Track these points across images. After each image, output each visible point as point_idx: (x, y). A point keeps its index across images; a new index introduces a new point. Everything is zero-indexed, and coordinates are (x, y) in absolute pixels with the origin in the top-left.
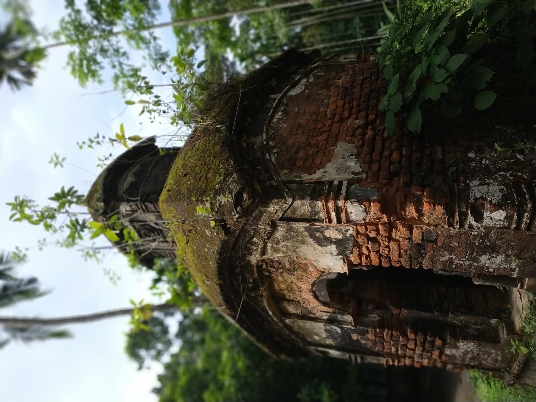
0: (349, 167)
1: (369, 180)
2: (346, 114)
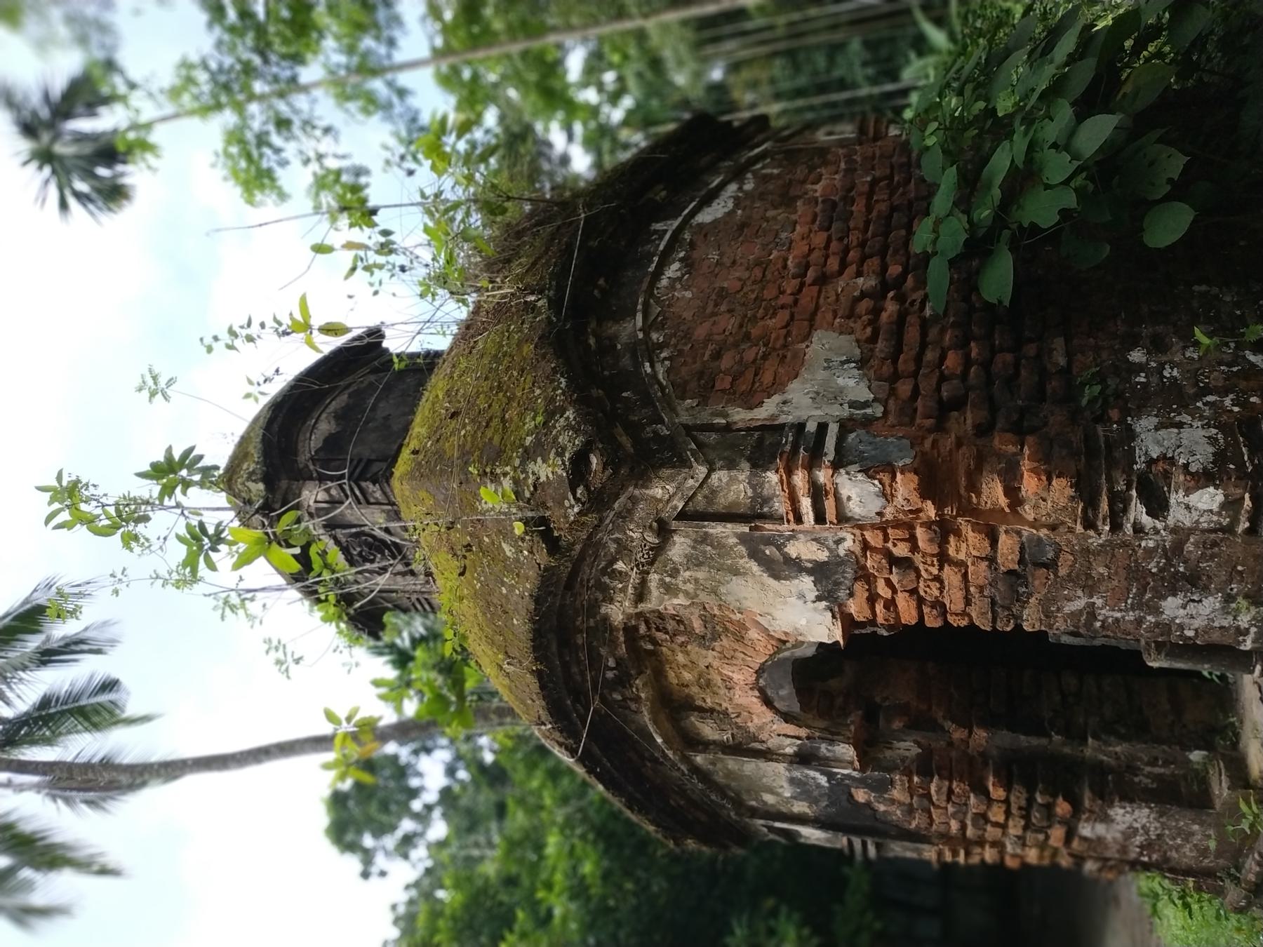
1: (891, 419)
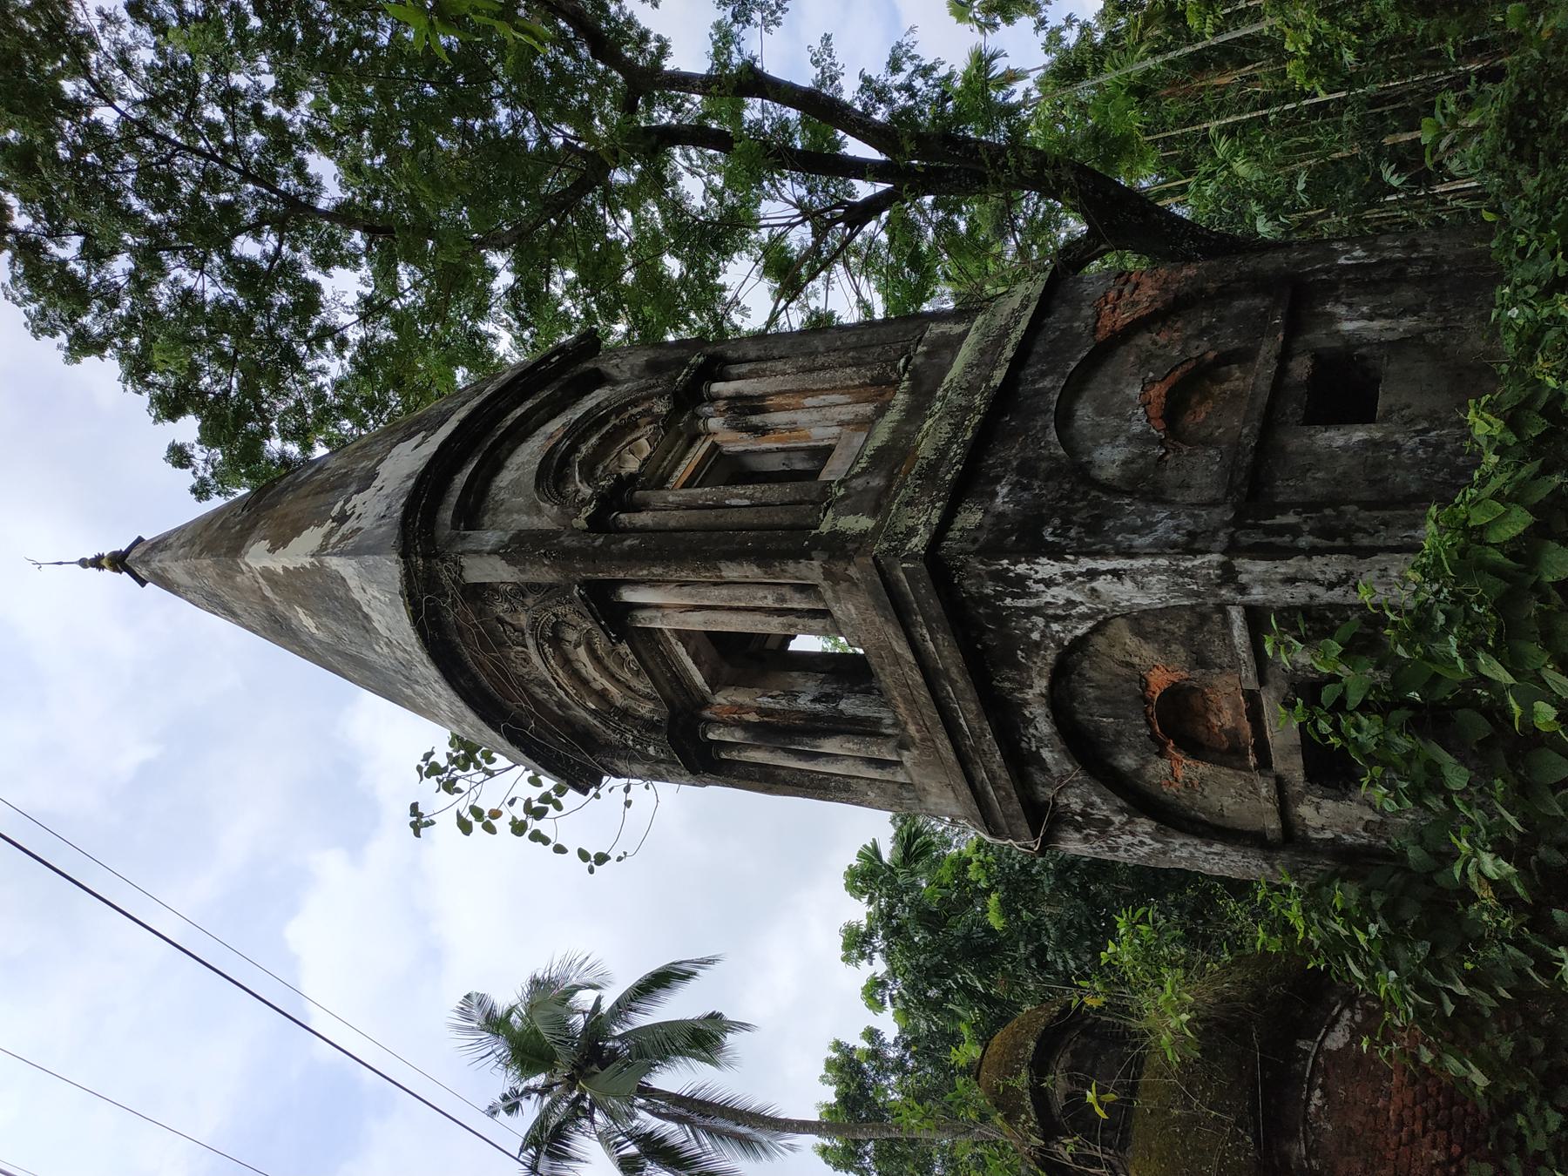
2: (1418, 1128)
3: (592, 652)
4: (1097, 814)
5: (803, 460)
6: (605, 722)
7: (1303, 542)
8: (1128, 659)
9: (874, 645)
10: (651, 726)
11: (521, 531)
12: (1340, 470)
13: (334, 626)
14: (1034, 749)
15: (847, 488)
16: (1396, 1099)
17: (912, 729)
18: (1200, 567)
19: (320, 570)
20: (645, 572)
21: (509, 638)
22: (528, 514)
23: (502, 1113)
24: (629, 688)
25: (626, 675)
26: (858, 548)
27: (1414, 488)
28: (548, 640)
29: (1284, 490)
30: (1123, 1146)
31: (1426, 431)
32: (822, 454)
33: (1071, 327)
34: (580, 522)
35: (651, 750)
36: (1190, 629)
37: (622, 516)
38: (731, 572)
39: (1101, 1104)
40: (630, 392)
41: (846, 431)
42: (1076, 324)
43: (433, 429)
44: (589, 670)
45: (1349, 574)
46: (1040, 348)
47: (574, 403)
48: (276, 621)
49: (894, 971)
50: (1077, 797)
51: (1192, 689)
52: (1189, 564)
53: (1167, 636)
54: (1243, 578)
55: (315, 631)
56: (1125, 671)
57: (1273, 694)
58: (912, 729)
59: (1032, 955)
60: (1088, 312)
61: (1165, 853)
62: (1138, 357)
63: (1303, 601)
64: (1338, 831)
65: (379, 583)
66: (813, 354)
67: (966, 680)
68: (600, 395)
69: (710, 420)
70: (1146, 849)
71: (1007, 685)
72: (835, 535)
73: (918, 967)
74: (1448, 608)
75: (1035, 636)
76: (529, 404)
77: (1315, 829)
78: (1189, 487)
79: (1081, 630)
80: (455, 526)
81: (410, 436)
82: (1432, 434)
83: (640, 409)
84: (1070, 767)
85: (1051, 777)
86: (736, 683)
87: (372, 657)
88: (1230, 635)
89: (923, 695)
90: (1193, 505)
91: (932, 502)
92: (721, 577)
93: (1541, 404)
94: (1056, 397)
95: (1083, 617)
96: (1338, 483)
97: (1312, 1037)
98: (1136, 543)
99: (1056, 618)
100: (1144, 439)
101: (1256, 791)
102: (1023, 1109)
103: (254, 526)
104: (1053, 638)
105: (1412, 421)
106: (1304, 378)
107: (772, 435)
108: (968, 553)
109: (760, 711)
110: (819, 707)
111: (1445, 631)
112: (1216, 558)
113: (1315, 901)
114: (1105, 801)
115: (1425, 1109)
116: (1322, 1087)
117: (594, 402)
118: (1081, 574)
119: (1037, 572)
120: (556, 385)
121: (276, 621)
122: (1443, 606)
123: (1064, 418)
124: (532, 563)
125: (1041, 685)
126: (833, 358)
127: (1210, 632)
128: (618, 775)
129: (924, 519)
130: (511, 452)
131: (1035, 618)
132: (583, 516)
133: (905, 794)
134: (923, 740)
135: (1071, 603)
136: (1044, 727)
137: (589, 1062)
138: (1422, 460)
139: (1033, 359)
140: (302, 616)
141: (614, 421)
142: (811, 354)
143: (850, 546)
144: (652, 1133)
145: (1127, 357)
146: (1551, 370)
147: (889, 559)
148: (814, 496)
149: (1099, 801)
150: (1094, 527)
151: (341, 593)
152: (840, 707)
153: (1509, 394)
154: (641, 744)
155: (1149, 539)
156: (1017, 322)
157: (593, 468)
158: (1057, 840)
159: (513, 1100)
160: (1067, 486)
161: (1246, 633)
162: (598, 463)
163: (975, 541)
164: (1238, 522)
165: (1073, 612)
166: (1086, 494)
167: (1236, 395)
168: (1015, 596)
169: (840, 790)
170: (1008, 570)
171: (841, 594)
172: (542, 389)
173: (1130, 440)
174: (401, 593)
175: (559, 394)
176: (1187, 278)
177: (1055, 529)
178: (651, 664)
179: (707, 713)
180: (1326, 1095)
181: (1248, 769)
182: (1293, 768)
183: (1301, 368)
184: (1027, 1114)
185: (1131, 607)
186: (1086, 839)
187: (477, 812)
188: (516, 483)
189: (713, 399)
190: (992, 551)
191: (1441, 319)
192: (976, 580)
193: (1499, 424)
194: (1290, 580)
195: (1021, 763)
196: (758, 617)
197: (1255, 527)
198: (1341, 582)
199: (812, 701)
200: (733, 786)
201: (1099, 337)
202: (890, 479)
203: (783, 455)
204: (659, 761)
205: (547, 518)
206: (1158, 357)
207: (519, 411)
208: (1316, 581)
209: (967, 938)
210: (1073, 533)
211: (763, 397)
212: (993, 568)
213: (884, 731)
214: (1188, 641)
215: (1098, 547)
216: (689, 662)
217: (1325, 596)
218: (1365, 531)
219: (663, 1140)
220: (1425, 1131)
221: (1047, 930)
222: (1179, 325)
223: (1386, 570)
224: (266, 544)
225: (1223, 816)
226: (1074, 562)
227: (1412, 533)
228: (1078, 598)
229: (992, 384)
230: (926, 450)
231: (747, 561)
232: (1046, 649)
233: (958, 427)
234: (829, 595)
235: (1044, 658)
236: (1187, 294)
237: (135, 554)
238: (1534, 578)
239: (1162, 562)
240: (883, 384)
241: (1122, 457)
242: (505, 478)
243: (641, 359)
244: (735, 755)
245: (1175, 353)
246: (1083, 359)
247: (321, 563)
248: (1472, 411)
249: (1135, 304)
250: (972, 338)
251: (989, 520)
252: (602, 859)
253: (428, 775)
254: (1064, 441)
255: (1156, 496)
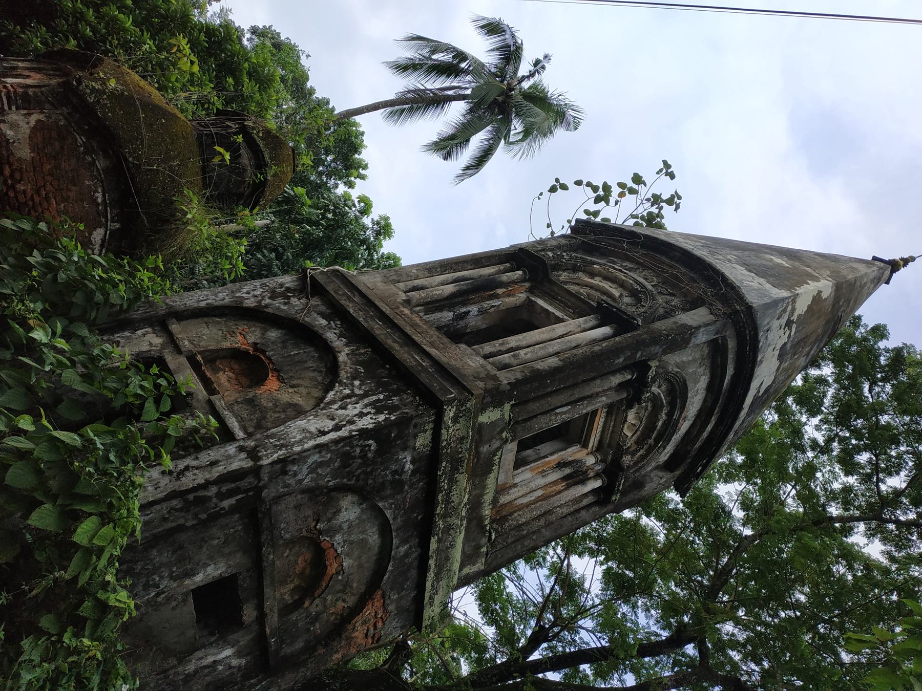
0: (10, 129)
2: (37, 199)
3: (610, 296)
4: (280, 300)
5: (528, 456)
6: (584, 260)
7: (214, 490)
8: (296, 389)
9: (449, 348)
10: (557, 267)
11: (686, 347)
12: (205, 549)
13: (764, 262)
14: (332, 322)
15: (502, 439)
16: (54, 213)
17: (407, 311)
18: (273, 454)
19: (789, 288)
20: (604, 345)
21: (662, 287)
22: (683, 362)
23: (542, 58)
24: (578, 284)
25: (583, 291)
26: (483, 399)
27: (155, 552)
28: (640, 292)
29: (236, 524)
30: (200, 137)
31: (157, 595)
32: (519, 463)
33: (398, 594)
34: (653, 364)
35: (551, 254)
36: (265, 418)
37: (629, 377)
38: (554, 362)
39: (220, 153)
40: (648, 463)
41: (511, 482)
42: (396, 596)
43: (756, 398)
44: (606, 285)
45: (178, 478)
46: (414, 573)
47: (677, 446)
48: (795, 257)
49: (357, 219)
50: (296, 305)
51: (250, 387)
52: (280, 453)
53: (277, 409)
54: (243, 455)
55: (772, 257)
56: (295, 382)
57: (200, 397)
58: (407, 311)
59: (283, 254)
60: (391, 608)
61: (233, 292)
62: (351, 587)
63: (201, 454)
64: (134, 336)
65: (754, 289)
66: (548, 525)
67: (388, 345)
68: (664, 457)
69: (594, 461)
70: (244, 291)
71: (362, 351)
72: (499, 404)
73: (344, 227)
74: (110, 466)
75: (357, 383)
76: (705, 434)
77: (148, 333)
78: (295, 507)
79: (331, 395)
80: (724, 338)
81: (767, 390)
82: (153, 594)
83: (639, 454)
84: (307, 319)
85: (315, 311)
86: (517, 308)
87: (734, 252)
88: (239, 422)
89: (409, 330)
90: (290, 494)
91: (449, 444)
92: (558, 357)
93: (89, 625)
94: (394, 542)
95: (333, 402)
96: (203, 540)
97: (112, 232)
98: (318, 456)
99: (348, 396)
100: (332, 531)
101: (191, 342)
102: (262, 139)
103: (834, 305)
104: (346, 385)
105: (169, 599)
106: (245, 607)
107: (554, 464)
108: (417, 416)
109: (497, 296)
110: (464, 310)
111: (107, 451)
112: (265, 462)
113: (137, 294)
114: (279, 308)
115: (36, 211)
116: (98, 204)
117: (666, 451)
118: (344, 426)
119: (371, 418)
120: (693, 453)
121: (795, 257)
122: (113, 466)
123: (385, 530)
124: (672, 329)
125: (342, 357)
126: (535, 526)
127: (251, 420)
128: (563, 236)
129: (451, 431)
130: (705, 401)
131: (361, 392)
132: (654, 368)
133: (395, 278)
134: (398, 308)
135: (343, 407)
136: (330, 336)
137: (504, 102)
138: (154, 574)
139: (416, 563)
140: (784, 263)
141: (651, 441)
142: (548, 525)
143: (488, 399)
144: (455, 77)
145: (358, 585)
146: (89, 650)
147: (463, 397)
148: (519, 428)
149: (282, 307)
150: (346, 458)
151: (771, 279)
152: (452, 313)
153: (111, 628)
154: (558, 255)
155: (310, 461)
156: (432, 585)
157: (654, 406)
158: (299, 279)
159: (538, 67)
160: (370, 482)
161: (230, 425)
162: (652, 411)
163: (415, 426)
164: (258, 490)
165: (340, 403)
166: (358, 480)
167: (283, 582)
168: (379, 401)
169: (433, 267)
170: (389, 414)
171: (481, 369)
172: (700, 447)
173: (341, 528)
174: (739, 287)
175: (689, 448)
176: (337, 652)
177: (369, 450)
178: (573, 300)
179: (527, 285)
180: (95, 200)
181: (200, 353)
182: (172, 361)
183: (249, 614)
184: (259, 137)
185: (306, 417)
186: (281, 285)
187: (632, 191)
188: (696, 381)
189: (597, 476)
190: (404, 422)
191: (171, 677)
192: (407, 404)
193: (112, 603)
194: (214, 464)
195: (336, 312)
196: (524, 343)
197: (246, 491)
198: (181, 473)
199: (469, 312)
200: (495, 251)
201: (380, 592)
202: (478, 453)
203: (542, 455)
204: (543, 250)
205: (673, 360)
206: (339, 592)
207: (709, 428)
208: (197, 468)
209: (322, 251)
210: (358, 450)
211: (568, 487)
212: (398, 413)
213: (421, 308)
214: (263, 411)
215: (340, 446)
216: (551, 309)
217: (189, 461)
218: (176, 510)
219: (448, 76)
220: (32, 199)
221: (279, 269)
222: (332, 618)
223: (156, 489)
224: (824, 295)
225: (206, 323)
226: (351, 431)
227: (146, 518)
228: (340, 412)
229: (436, 537)
230: (463, 479)
231: (546, 371)
232: (347, 378)
233: (448, 501)
234: (489, 367)
235: (347, 372)
236: (334, 640)
237: (888, 273)
238: (59, 502)
239: (297, 449)
240: (500, 519)
241: (342, 515)
242: (703, 382)
243: (648, 488)
244: (501, 267)
245: (329, 598)
246: (385, 574)
247: (792, 292)
248: (132, 606)
249: (364, 623)
250: (456, 566)
251: (411, 443)
252: (553, 190)
253: (673, 197)
254: (380, 513)
255: (312, 492)
